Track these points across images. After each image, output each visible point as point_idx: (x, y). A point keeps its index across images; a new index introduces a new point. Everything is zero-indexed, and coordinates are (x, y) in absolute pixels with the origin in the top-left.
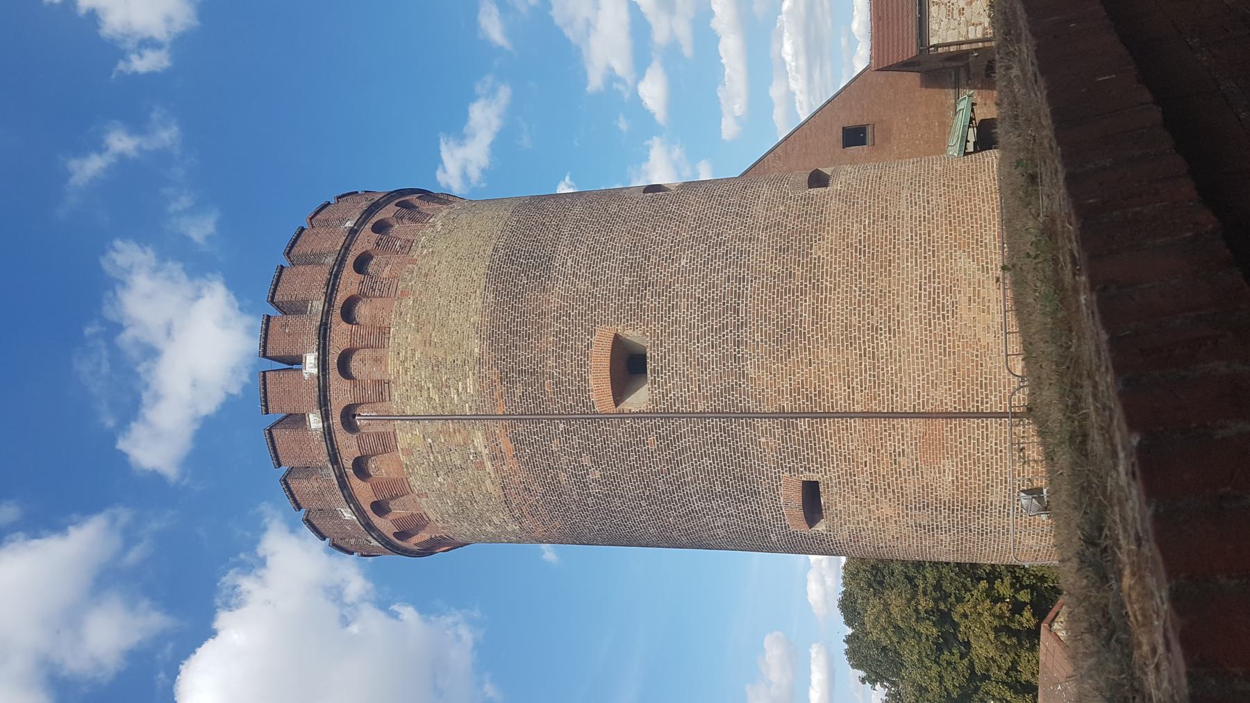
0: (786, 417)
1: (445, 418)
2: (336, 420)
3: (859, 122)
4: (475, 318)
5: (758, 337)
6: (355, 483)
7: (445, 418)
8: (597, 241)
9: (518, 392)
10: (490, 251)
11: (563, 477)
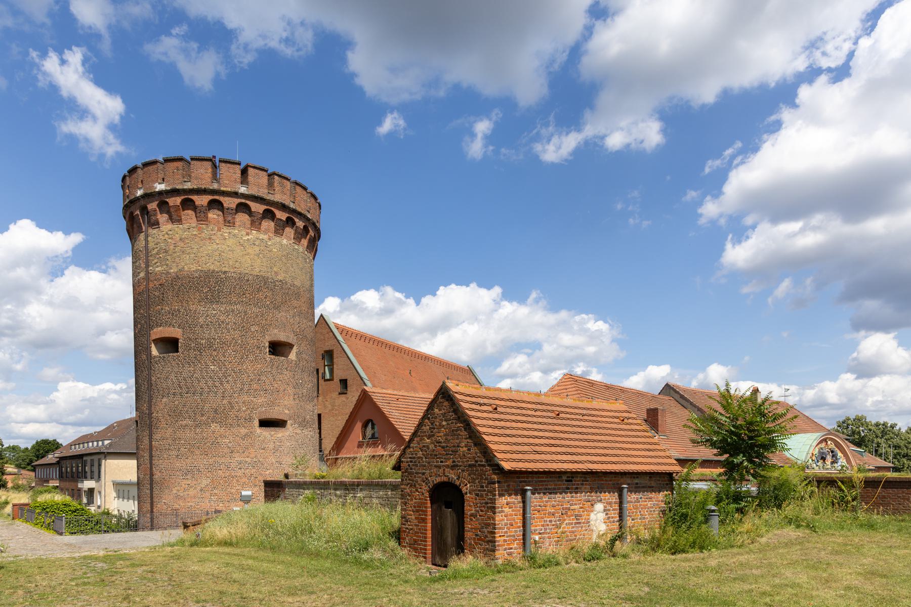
3: (438, 387)
4: (186, 268)
5: (176, 403)
8: (228, 324)
10: (224, 269)
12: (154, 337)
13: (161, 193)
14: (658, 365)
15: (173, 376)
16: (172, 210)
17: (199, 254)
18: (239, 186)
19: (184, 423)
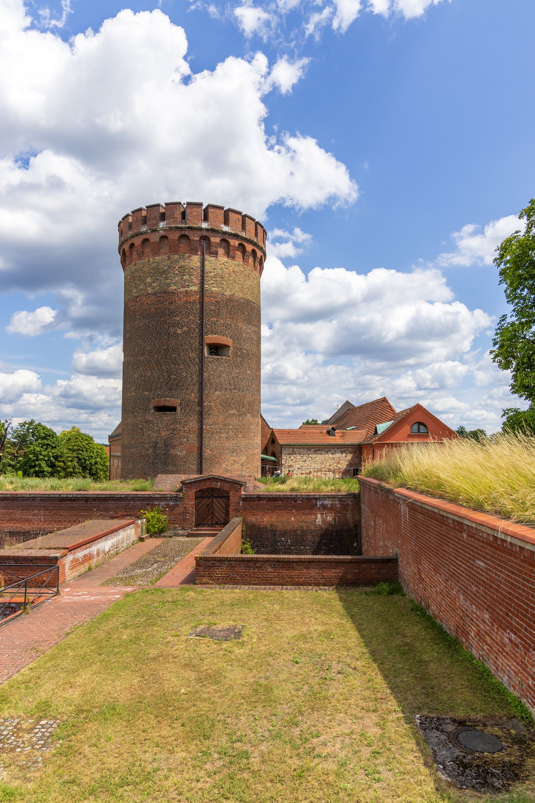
0: (201, 403)
1: (203, 277)
2: (205, 233)
6: (177, 235)
7: (203, 277)
9: (212, 307)
11: (178, 318)
12: (209, 341)
13: (225, 233)
14: (64, 380)
15: (224, 375)
16: (231, 248)
17: (244, 286)
18: (223, 226)
19: (232, 412)
